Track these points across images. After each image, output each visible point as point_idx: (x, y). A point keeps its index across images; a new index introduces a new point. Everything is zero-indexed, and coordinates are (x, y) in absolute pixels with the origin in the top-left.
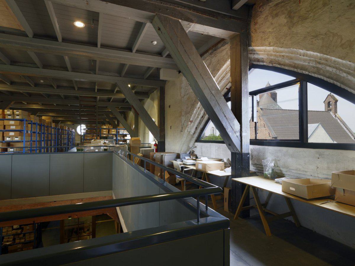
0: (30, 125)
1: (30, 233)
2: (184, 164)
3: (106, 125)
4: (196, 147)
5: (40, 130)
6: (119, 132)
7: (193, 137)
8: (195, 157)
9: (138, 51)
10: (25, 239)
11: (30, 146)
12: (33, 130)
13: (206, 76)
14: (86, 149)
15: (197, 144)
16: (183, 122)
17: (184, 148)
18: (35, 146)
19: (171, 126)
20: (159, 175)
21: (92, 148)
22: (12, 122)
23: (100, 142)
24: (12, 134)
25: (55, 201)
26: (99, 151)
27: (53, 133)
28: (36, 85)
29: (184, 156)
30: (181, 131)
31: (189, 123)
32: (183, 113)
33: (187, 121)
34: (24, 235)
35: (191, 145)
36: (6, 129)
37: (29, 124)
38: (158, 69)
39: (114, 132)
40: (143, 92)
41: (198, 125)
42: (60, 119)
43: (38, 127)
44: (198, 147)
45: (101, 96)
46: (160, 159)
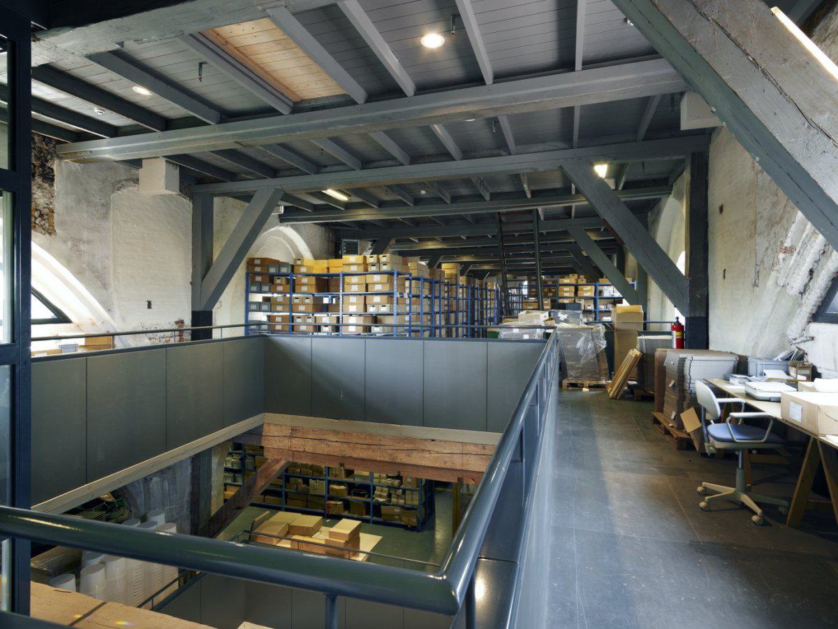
0: (407, 283)
1: (412, 490)
2: (749, 396)
3: (571, 275)
4: (813, 338)
5: (431, 290)
6: (601, 292)
7: (800, 305)
8: (808, 372)
9: (588, 64)
10: (405, 499)
11: (408, 324)
12: (414, 292)
13: (785, 60)
14: (503, 333)
15: (816, 328)
16: (760, 256)
17: (768, 341)
18: (419, 323)
19: (725, 271)
20: (673, 417)
21: (516, 331)
22: (377, 278)
23: (538, 317)
24: (377, 299)
25: (433, 440)
26: (532, 338)
27: (460, 296)
28: (418, 201)
29: (759, 367)
30: (755, 285)
31: (781, 256)
32: (761, 225)
33: (772, 250)
34: (404, 491)
35: (794, 330)
36: (369, 290)
37: (407, 279)
38: (673, 100)
39: (588, 291)
40: (654, 180)
41: (817, 262)
42: (486, 267)
43: (427, 284)
44: (818, 338)
45: (547, 207)
46: (676, 367)
